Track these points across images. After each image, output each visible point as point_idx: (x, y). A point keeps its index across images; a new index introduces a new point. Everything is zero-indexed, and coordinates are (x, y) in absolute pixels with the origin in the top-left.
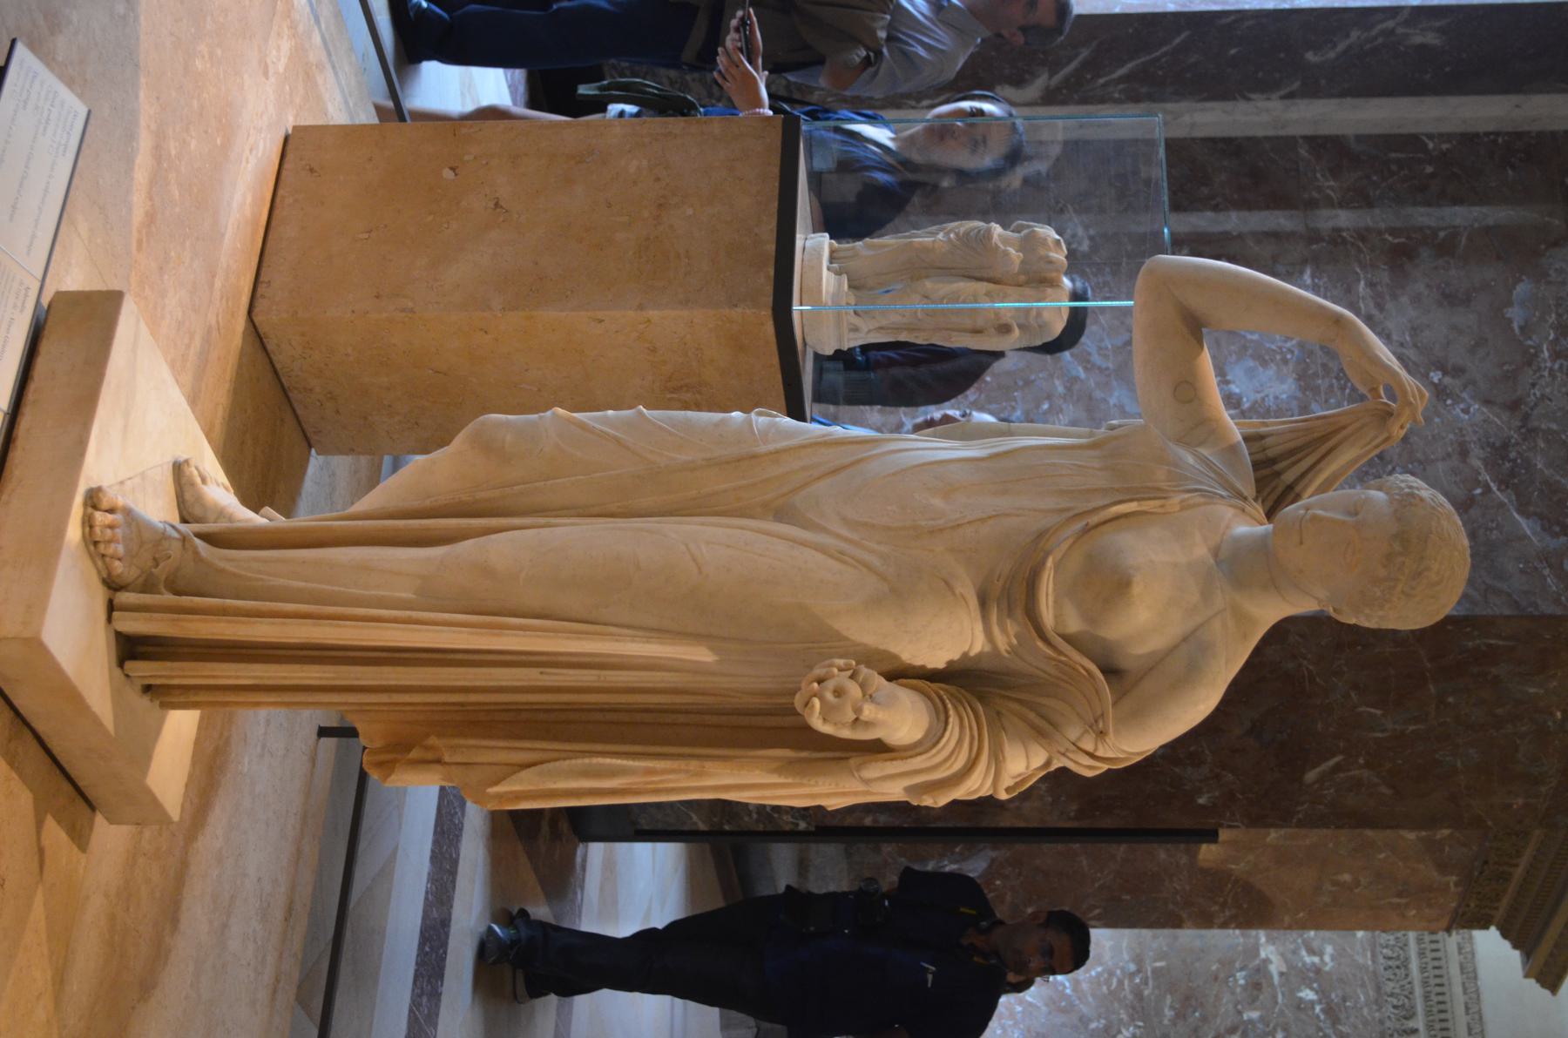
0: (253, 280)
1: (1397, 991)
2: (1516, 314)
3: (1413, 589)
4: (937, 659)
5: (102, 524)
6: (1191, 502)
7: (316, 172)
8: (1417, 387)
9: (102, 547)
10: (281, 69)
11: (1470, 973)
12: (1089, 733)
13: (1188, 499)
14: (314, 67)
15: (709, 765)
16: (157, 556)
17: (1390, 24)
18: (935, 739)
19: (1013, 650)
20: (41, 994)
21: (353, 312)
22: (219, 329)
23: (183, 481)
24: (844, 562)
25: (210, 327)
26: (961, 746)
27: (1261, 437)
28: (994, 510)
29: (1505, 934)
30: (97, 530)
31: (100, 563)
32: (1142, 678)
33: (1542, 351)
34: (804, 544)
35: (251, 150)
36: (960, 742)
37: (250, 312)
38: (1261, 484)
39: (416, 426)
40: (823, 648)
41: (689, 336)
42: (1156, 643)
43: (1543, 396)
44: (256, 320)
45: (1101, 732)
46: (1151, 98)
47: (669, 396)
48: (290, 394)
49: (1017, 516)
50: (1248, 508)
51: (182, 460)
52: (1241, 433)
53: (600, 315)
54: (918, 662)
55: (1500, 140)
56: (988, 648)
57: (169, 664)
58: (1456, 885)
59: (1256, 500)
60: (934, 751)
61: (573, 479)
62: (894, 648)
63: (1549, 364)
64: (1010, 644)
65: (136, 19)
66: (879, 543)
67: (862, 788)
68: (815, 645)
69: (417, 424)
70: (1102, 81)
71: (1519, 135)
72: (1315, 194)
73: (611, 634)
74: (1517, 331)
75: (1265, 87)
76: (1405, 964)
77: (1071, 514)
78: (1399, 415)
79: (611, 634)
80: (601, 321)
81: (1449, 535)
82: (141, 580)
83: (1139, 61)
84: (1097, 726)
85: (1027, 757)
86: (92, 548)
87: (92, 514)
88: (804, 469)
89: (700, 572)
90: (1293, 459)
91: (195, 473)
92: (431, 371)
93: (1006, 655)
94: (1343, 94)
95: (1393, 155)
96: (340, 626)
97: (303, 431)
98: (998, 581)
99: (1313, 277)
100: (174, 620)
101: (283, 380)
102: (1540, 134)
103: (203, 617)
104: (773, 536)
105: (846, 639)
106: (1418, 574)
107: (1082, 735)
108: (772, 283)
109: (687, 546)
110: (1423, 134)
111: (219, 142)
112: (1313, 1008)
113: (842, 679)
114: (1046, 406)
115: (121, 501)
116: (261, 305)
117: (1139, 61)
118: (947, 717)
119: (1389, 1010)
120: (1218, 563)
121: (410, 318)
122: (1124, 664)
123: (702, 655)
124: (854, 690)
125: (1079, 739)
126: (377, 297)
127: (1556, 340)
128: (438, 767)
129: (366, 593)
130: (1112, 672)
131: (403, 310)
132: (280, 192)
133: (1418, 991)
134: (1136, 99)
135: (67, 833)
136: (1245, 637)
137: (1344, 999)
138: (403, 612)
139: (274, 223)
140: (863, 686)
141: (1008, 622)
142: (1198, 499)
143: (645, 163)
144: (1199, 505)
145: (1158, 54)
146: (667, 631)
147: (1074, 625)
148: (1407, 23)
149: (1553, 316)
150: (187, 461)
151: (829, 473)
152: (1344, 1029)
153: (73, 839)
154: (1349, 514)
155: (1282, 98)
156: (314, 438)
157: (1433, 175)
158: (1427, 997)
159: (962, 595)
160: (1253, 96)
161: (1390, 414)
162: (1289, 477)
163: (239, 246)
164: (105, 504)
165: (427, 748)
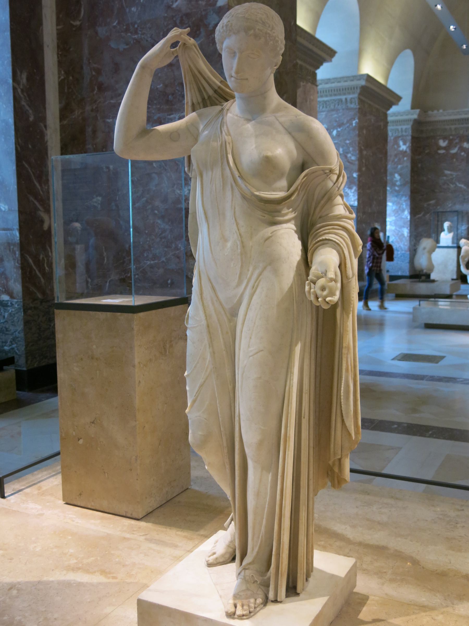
0: (125, 518)
1: (333, 104)
2: (122, 47)
3: (269, 27)
4: (298, 245)
5: (241, 611)
6: (226, 131)
7: (81, 493)
8: (173, 31)
9: (251, 610)
10: (39, 507)
11: (328, 81)
12: (331, 176)
13: (225, 132)
14: (40, 491)
15: (344, 345)
16: (252, 582)
17: (19, 90)
18: (336, 245)
19: (294, 210)
20: (432, 618)
21: (137, 480)
22: (146, 535)
23: (215, 562)
24: (258, 286)
25: (146, 539)
26: (338, 233)
27: (193, 104)
28: (233, 219)
29: (318, 68)
30: (244, 613)
31: (258, 609)
32: (307, 152)
33: (135, 38)
34: (249, 304)
35: (73, 521)
36: (336, 234)
37: (138, 520)
38: (213, 104)
39: (180, 450)
40: (296, 295)
41: (145, 347)
42: (292, 146)
43: (151, 37)
44: (141, 517)
45: (330, 171)
46: (47, 175)
47: (168, 353)
48: (169, 499)
49: (235, 208)
50: (227, 108)
51: (206, 563)
52: (191, 113)
53: (137, 382)
54: (300, 253)
55: (60, 53)
56: (293, 222)
57: (299, 575)
58: (303, 82)
59: (222, 105)
60: (342, 245)
61: (218, 405)
62: (295, 264)
63: (140, 35)
64: (292, 212)
65: (19, 583)
66: (248, 270)
67: (354, 277)
68: (295, 299)
69: (179, 449)
70: (41, 193)
71: (58, 47)
72: (80, 118)
73: (290, 388)
74: (128, 47)
75: (42, 135)
76: (325, 102)
77: (234, 184)
78: (185, 40)
79: (290, 388)
80: (140, 382)
81: (245, 9)
82: (262, 587)
83: (34, 179)
84: (328, 173)
85: (339, 205)
86: (252, 614)
87: (237, 615)
88: (213, 304)
89: (262, 351)
90: (203, 90)
91: (212, 557)
92: (160, 447)
93: (296, 213)
94: (45, 108)
95: (66, 91)
96: (285, 507)
97: (182, 492)
98: (265, 217)
99: (109, 119)
100: (281, 576)
101: (163, 503)
102: (58, 39)
103: (280, 563)
104: (245, 319)
105: (292, 285)
106: (264, 23)
107: (331, 180)
108: (122, 314)
109: (250, 357)
110: (58, 80)
111: (70, 538)
112: (339, 131)
113: (316, 289)
114: (156, 212)
115: (231, 602)
116: (135, 515)
117: (34, 179)
118: (326, 239)
119: (340, 107)
120: (254, 120)
121: (139, 457)
122: (300, 161)
123: (298, 349)
124: (321, 282)
125: (332, 181)
126: (131, 470)
127: (131, 33)
128: (342, 460)
129: (269, 493)
130: (303, 167)
131: (136, 460)
132: (89, 507)
133: (333, 98)
134: (48, 180)
135: (363, 606)
136: (286, 108)
137: (336, 121)
138: (279, 479)
139: (102, 510)
140: (319, 278)
141: (283, 212)
142: (225, 128)
143: (75, 364)
144: (227, 127)
145: (31, 173)
146: (288, 364)
147: (283, 183)
148: (19, 84)
149: (122, 34)
150: (207, 562)
151: (215, 293)
152: (345, 121)
153: (365, 603)
154: (234, 56)
155: (46, 129)
156: (185, 488)
157: (73, 77)
158: (335, 95)
159: (271, 233)
160: (46, 140)
161: (185, 44)
162: (211, 92)
163: (112, 526)
164: (232, 609)
165: (334, 464)
